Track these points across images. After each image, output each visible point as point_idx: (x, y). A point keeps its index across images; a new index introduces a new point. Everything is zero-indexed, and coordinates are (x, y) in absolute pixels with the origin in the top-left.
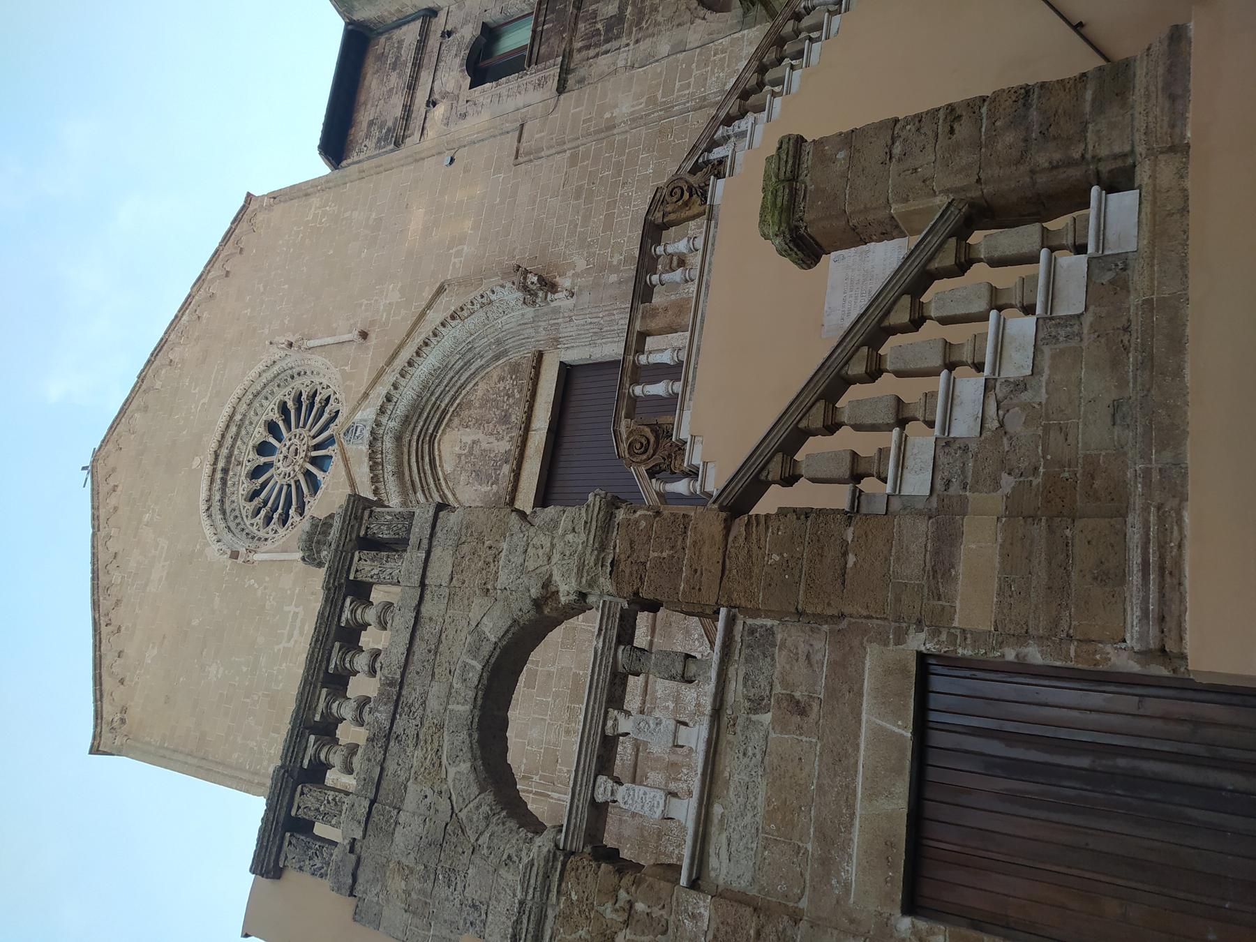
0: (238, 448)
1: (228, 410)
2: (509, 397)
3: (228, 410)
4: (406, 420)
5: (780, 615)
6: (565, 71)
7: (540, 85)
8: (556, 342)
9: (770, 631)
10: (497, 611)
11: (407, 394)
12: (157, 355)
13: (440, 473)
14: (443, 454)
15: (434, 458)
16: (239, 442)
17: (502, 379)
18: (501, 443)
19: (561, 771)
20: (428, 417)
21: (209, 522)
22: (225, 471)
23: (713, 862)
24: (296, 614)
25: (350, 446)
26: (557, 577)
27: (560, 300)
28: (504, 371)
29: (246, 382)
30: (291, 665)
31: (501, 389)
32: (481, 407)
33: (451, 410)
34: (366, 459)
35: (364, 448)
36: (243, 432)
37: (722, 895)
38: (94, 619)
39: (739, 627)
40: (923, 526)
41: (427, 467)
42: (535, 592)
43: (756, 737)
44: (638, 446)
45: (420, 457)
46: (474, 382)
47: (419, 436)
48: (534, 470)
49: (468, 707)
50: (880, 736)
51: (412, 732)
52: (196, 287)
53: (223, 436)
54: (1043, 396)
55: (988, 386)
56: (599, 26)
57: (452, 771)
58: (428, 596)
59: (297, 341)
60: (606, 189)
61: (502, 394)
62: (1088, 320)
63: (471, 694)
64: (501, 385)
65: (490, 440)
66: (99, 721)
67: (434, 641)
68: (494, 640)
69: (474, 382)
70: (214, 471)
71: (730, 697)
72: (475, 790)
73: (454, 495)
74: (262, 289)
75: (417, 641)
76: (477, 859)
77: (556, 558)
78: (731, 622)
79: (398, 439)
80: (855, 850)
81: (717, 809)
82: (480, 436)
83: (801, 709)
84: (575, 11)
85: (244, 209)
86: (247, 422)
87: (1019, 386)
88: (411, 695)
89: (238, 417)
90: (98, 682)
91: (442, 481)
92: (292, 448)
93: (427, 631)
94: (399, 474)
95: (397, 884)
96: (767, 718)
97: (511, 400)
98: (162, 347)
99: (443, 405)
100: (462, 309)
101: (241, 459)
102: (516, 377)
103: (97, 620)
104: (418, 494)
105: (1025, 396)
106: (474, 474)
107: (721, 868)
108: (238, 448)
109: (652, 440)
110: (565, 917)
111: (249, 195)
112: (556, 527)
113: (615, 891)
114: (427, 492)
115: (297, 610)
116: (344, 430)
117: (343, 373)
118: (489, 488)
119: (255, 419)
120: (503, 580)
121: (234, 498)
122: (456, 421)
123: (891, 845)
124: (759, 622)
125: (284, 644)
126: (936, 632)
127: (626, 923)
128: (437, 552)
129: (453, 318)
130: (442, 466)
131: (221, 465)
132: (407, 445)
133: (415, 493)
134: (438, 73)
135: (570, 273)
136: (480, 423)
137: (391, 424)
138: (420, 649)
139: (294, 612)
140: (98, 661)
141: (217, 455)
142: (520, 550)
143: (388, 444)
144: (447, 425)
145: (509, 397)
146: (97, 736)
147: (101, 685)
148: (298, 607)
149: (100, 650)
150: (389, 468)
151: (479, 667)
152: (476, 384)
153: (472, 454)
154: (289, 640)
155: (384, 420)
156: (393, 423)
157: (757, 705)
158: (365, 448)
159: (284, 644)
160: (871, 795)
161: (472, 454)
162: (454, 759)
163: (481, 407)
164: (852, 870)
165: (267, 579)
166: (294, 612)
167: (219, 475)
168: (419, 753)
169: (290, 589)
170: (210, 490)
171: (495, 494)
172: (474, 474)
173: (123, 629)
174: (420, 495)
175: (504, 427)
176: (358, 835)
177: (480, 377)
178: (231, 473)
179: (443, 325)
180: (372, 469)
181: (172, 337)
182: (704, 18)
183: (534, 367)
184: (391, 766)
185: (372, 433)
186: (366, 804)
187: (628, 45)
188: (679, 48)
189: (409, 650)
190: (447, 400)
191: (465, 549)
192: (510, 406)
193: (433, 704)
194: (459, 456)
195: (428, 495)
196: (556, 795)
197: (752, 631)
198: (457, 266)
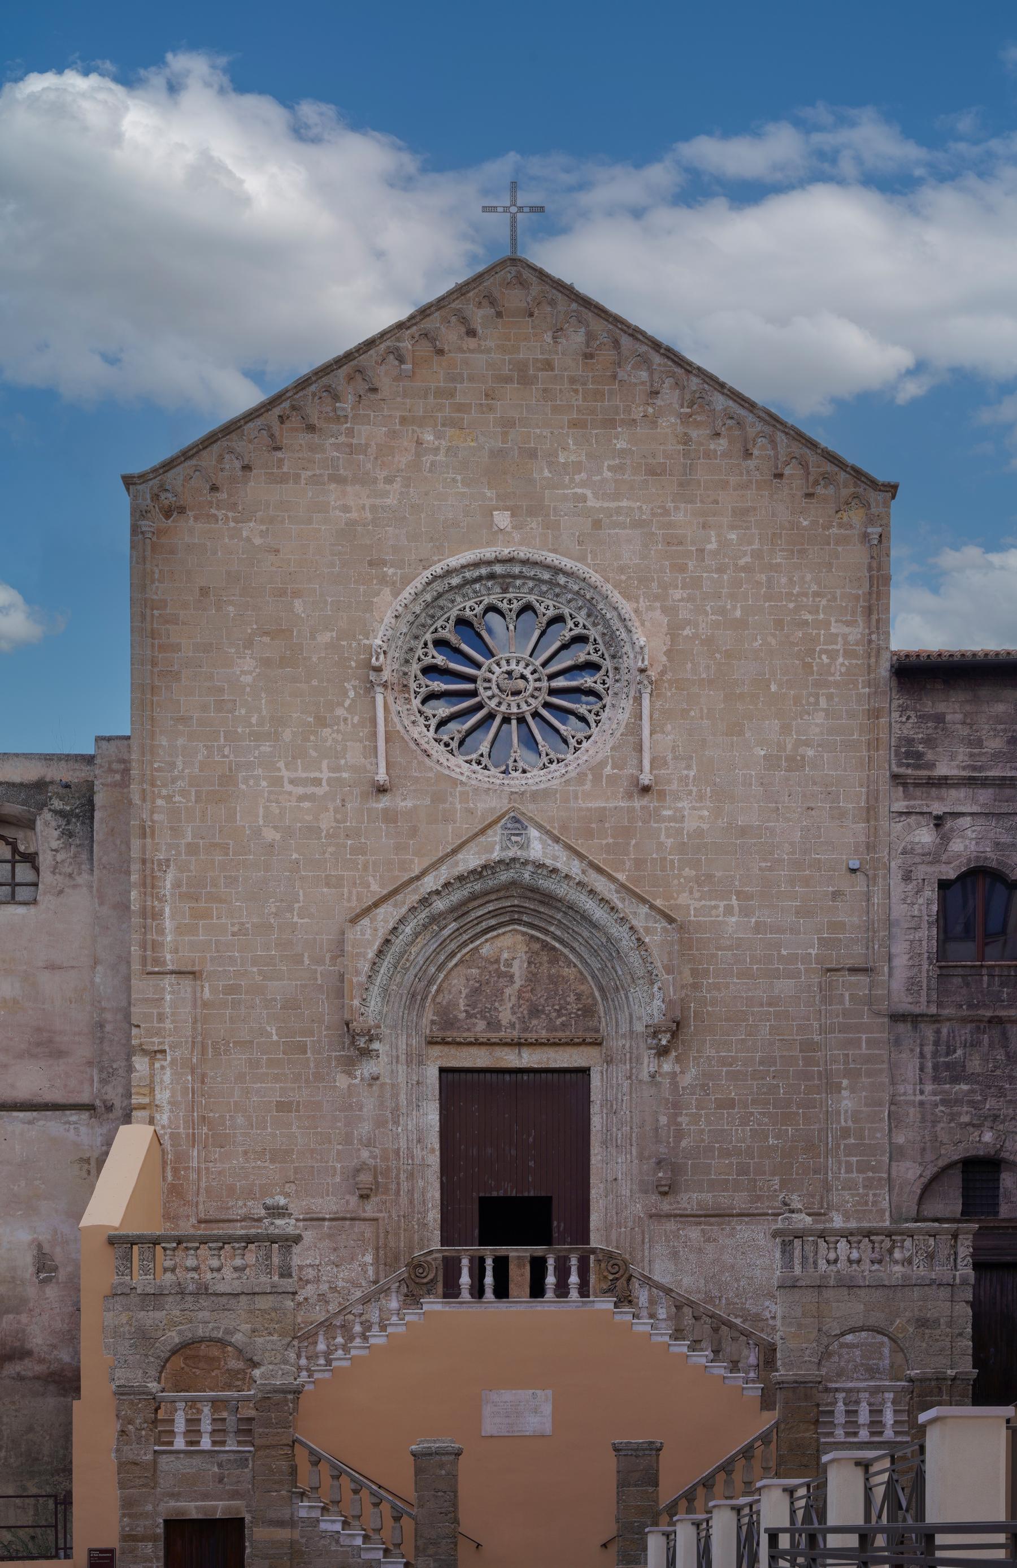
0: (524, 584)
1: (569, 566)
2: (558, 1011)
3: (569, 566)
4: (534, 890)
5: (253, 1469)
6: (915, 1019)
7: (912, 985)
8: (609, 1061)
9: (247, 1467)
10: (245, 1339)
11: (561, 890)
12: (668, 357)
13: (478, 942)
14: (502, 938)
15: (495, 929)
16: (531, 584)
17: (579, 997)
18: (509, 1011)
19: (215, 1152)
20: (540, 912)
21: (420, 587)
22: (492, 576)
23: (164, 1456)
24: (317, 782)
25: (499, 831)
26: (263, 1369)
27: (648, 1064)
28: (588, 998)
29: (604, 589)
30: (266, 795)
31: (568, 999)
32: (550, 977)
33: (548, 939)
34: (482, 862)
35: (495, 854)
36: (544, 588)
37: (155, 1462)
38: (286, 391)
39: (248, 1455)
40: (287, 1517)
41: (484, 925)
42: (255, 1358)
43: (209, 1466)
44: (421, 1271)
45: (496, 913)
46: (578, 963)
47: (518, 906)
48: (478, 1060)
49: (202, 1335)
50: (216, 1507)
51: (187, 1306)
52: (763, 415)
53: (535, 564)
54: (333, 1549)
55: (338, 1532)
56: (959, 1052)
57: (174, 1334)
58: (249, 1297)
59: (648, 677)
60: (764, 1093)
61: (562, 1002)
62: (359, 1560)
63: (207, 1335)
64: (572, 998)
65: (513, 998)
66: (161, 471)
67: (228, 1307)
68: (233, 1340)
69: (578, 963)
70: (489, 563)
71: (221, 1455)
72: (169, 1348)
73: (456, 965)
74: (742, 562)
75: (227, 1297)
76: (143, 1358)
77: (271, 1367)
78: (249, 1452)
79: (513, 883)
80: (179, 1504)
81: (182, 1456)
82: (518, 982)
83: (221, 1481)
84: (986, 1019)
85: (873, 484)
86: (557, 590)
87: (337, 1541)
88: (204, 1302)
89: (562, 580)
90: (206, 443)
91: (471, 946)
92: (521, 683)
93: (233, 1301)
94: (473, 897)
95: (124, 1319)
96: (216, 1469)
97: (554, 1014)
98: (680, 365)
99: (552, 929)
100: (646, 951)
101: (511, 590)
102: (578, 1016)
103: (283, 398)
104: (454, 924)
105: (334, 1543)
106: (477, 985)
107: (163, 1459)
108: (524, 584)
109: (425, 1281)
110: (132, 1403)
111: (892, 489)
112: (285, 1364)
113: (145, 1422)
114: (457, 933)
115: (324, 783)
116: (519, 816)
117: (602, 764)
118: (463, 1009)
119: (562, 600)
120: (260, 1340)
121: (459, 599)
122: (537, 946)
123: (183, 1514)
124: (250, 1462)
125: (285, 773)
126: (252, 1522)
127: (137, 1429)
128: (271, 1298)
129: (638, 939)
130: (487, 941)
131: (498, 569)
132: (508, 894)
133: (455, 920)
134: (981, 821)
135: (678, 1069)
136: (532, 978)
137: (527, 876)
138: (223, 1300)
139: (321, 780)
140: (233, 427)
141: (511, 560)
142: (274, 1347)
143: (504, 877)
144: (532, 937)
145: (558, 1011)
146: (143, 477)
147: (205, 448)
148: (329, 785)
149: (246, 423)
150: (478, 887)
151: (220, 1336)
152: (575, 966)
153: (499, 978)
154: (292, 782)
155: (530, 868)
156: (528, 878)
157: (220, 1465)
158: (496, 855)
159: (285, 773)
160: (196, 1507)
161: (499, 978)
162: (180, 1332)
163: (550, 977)
164: (172, 1503)
165: (356, 719)
166: (321, 780)
167: (484, 571)
168: (178, 1313)
169: (346, 762)
170: (463, 567)
171: (455, 1017)
172: (477, 985)
173: (279, 454)
174: (454, 926)
175: (525, 1012)
176: (139, 1291)
177: (583, 969)
178: (490, 584)
179: (631, 928)
180: (473, 872)
181: (695, 380)
182: (921, 1176)
183: (584, 1040)
184: (170, 1299)
185: (514, 860)
186: (152, 1292)
187: (922, 1092)
188: (896, 1153)
189: (222, 1294)
190: (558, 933)
191: (273, 1314)
192: (548, 1015)
193: (201, 1315)
194: (497, 961)
195: (453, 936)
196: (195, 1153)
197: (247, 1460)
198: (714, 912)
